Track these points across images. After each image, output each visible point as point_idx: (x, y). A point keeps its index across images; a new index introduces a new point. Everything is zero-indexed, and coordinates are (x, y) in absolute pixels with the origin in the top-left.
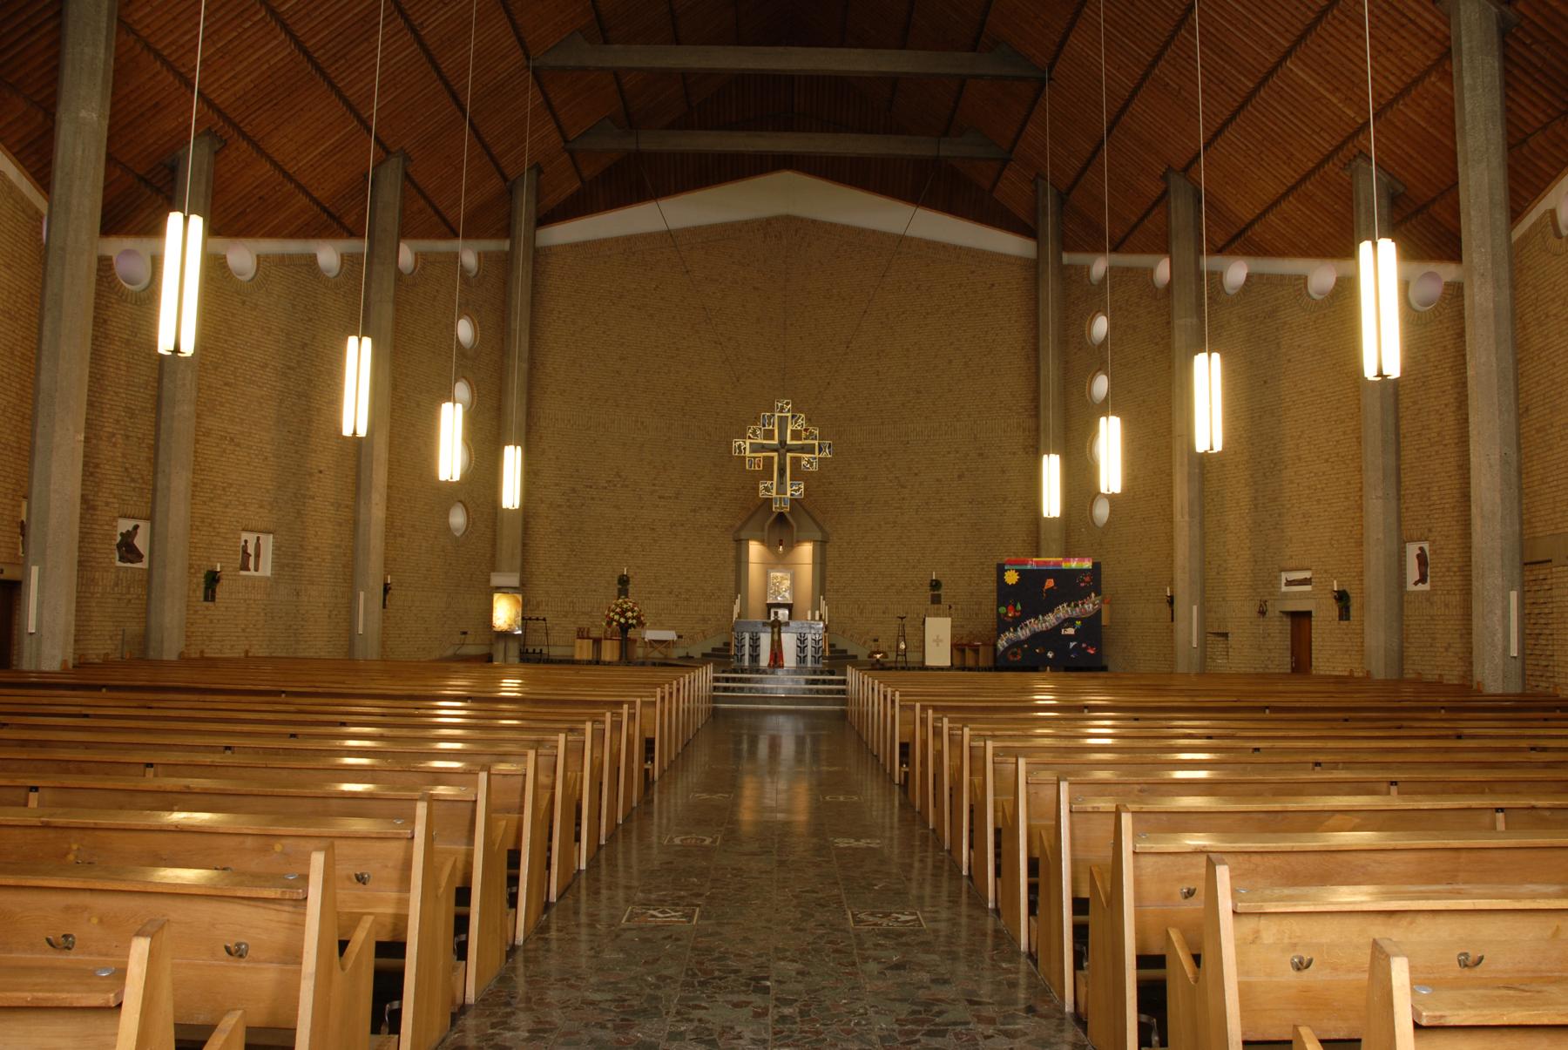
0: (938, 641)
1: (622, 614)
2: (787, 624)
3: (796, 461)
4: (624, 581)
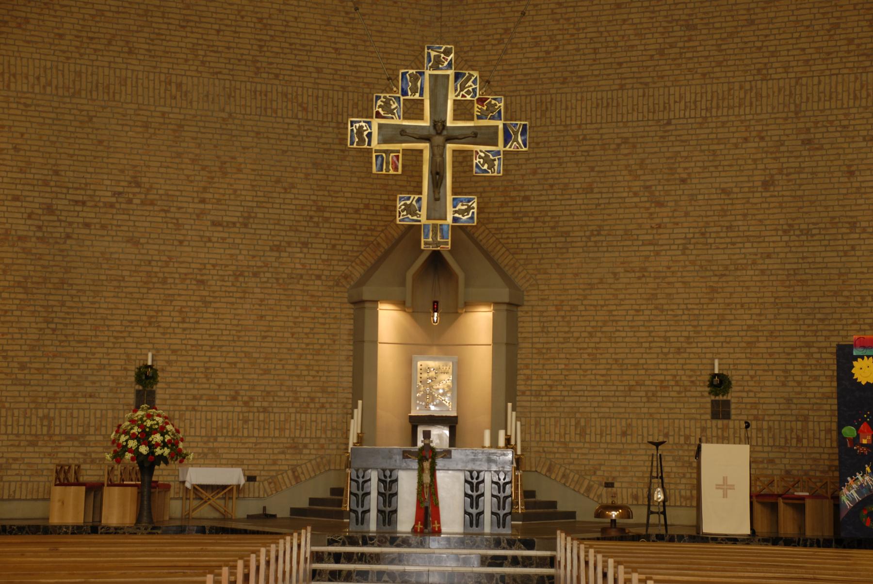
0: (725, 487)
1: (144, 437)
2: (447, 454)
3: (463, 159)
4: (146, 377)
